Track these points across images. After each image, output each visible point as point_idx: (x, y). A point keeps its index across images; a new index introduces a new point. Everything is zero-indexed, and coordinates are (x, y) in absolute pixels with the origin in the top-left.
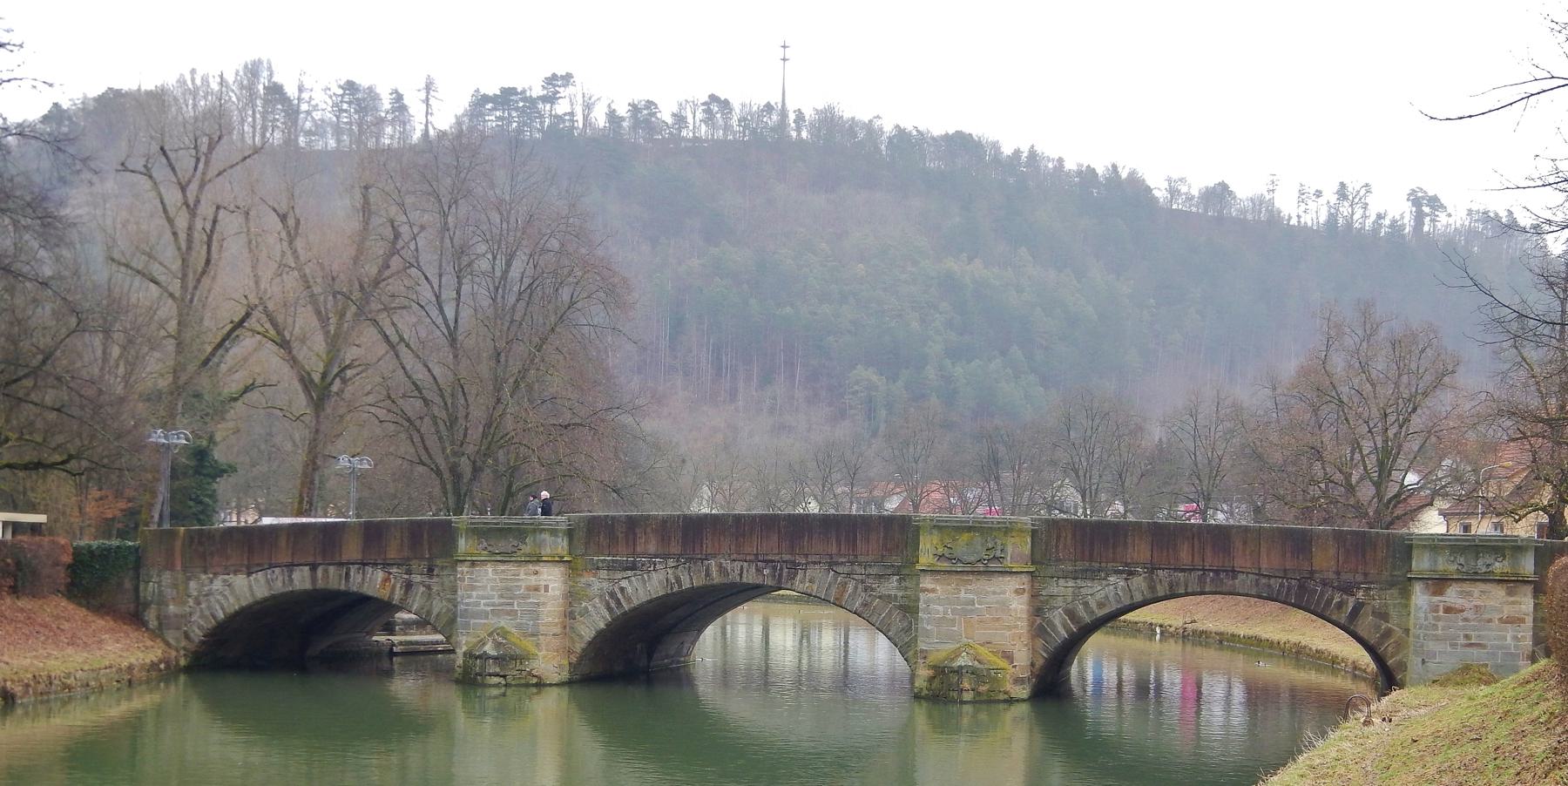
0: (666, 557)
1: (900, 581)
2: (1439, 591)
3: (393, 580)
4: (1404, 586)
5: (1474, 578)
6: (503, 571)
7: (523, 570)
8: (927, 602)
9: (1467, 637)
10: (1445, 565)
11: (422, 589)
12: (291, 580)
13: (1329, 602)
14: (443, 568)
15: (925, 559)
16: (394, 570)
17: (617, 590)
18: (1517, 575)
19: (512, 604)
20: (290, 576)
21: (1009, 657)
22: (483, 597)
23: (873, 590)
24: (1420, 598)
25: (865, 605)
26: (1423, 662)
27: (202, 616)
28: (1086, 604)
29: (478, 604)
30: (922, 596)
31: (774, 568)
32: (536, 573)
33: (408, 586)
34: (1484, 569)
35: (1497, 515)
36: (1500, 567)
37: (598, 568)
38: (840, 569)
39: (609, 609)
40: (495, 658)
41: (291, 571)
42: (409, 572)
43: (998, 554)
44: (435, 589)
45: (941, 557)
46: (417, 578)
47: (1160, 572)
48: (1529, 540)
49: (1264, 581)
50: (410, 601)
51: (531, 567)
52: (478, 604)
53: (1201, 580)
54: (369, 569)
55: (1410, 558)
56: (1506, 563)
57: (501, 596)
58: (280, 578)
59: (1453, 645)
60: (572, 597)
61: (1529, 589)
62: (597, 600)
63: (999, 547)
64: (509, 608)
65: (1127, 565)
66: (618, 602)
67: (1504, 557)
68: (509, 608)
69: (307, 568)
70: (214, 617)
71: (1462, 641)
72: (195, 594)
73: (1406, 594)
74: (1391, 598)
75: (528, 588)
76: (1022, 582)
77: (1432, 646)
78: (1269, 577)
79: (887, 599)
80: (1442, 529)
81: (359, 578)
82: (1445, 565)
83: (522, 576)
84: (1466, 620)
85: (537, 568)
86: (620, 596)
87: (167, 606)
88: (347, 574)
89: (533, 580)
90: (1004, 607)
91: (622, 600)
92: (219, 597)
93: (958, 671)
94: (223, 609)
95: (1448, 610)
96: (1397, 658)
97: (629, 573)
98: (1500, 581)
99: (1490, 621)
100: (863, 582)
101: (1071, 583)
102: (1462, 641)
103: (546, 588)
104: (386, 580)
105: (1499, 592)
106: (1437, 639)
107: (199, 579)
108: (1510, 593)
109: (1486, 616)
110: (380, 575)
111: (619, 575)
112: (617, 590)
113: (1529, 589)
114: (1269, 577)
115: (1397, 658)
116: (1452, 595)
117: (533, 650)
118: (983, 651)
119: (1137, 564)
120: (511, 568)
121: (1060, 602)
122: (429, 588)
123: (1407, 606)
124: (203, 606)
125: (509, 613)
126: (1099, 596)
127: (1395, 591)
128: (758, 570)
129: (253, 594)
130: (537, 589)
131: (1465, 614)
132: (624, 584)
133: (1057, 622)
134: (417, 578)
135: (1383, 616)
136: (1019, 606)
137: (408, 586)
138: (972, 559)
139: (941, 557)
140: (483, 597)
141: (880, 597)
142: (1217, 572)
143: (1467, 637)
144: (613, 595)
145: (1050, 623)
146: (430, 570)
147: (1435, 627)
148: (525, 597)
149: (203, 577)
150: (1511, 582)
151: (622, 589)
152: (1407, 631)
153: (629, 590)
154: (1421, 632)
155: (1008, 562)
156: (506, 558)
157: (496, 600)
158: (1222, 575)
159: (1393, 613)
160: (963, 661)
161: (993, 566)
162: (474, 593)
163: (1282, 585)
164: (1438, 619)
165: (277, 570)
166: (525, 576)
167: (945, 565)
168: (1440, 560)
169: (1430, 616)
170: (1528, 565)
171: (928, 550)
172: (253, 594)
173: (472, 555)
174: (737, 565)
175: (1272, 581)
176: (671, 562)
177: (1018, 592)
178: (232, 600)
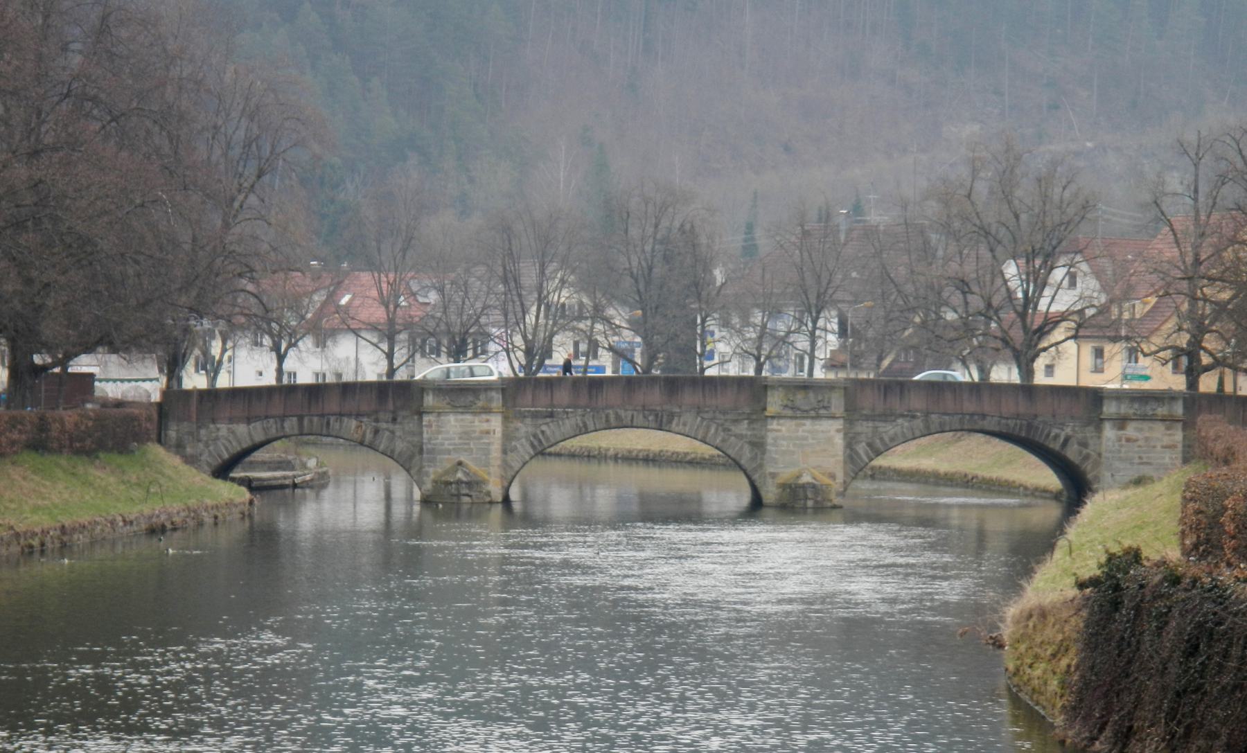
0: (576, 407)
1: (749, 424)
2: (1122, 428)
3: (364, 427)
4: (1098, 422)
5: (1144, 418)
6: (462, 420)
7: (477, 419)
8: (775, 439)
9: (1140, 458)
10: (1125, 409)
11: (387, 433)
12: (283, 428)
13: (1048, 435)
14: (404, 418)
15: (772, 409)
16: (365, 419)
17: (538, 432)
18: (1172, 416)
19: (469, 444)
20: (282, 425)
21: (833, 476)
22: (447, 439)
23: (729, 430)
24: (1109, 432)
25: (723, 441)
26: (1112, 475)
27: (210, 454)
28: (882, 439)
29: (442, 444)
30: (769, 434)
31: (657, 416)
32: (488, 421)
33: (376, 432)
34: (1151, 413)
35: (96, 246)
36: (1162, 411)
37: (525, 417)
38: (706, 416)
39: (533, 446)
40: (467, 483)
41: (283, 421)
42: (377, 420)
43: (826, 404)
44: (398, 434)
45: (786, 406)
46: (383, 425)
47: (933, 416)
48: (1180, 392)
49: (1004, 421)
50: (377, 442)
51: (484, 417)
52: (442, 444)
53: (961, 421)
54: (345, 419)
55: (1101, 405)
56: (1165, 408)
57: (460, 438)
58: (274, 426)
59: (1132, 464)
60: (508, 437)
61: (1180, 425)
62: (524, 440)
63: (826, 400)
64: (466, 447)
65: (909, 411)
66: (540, 441)
67: (1164, 404)
68: (466, 447)
69: (295, 419)
70: (220, 456)
71: (1137, 461)
72: (205, 439)
73: (1099, 429)
74: (1090, 432)
75: (482, 432)
76: (839, 424)
77: (1117, 464)
78: (1007, 418)
79: (740, 437)
80: (822, 376)
81: (337, 426)
82: (1125, 409)
83: (477, 423)
84: (1139, 446)
85: (488, 417)
86: (541, 436)
87: (185, 448)
88: (328, 423)
89: (485, 426)
90: (830, 440)
91: (543, 440)
92: (224, 441)
93: (803, 486)
94: (227, 449)
95: (1128, 440)
96: (1095, 473)
97: (548, 420)
98: (1161, 420)
99: (1154, 447)
100: (722, 425)
101: (870, 424)
102: (1137, 461)
103: (494, 431)
104: (358, 427)
105: (1160, 427)
106: (1120, 459)
107: (208, 427)
108: (1168, 428)
109: (1152, 444)
110: (354, 423)
111: (540, 421)
112: (538, 432)
113: (1180, 425)
114: (1007, 418)
115: (1095, 473)
116: (1131, 430)
117: (486, 477)
118: (816, 473)
119: (917, 411)
120: (468, 417)
121: (863, 437)
122: (393, 432)
123: (1099, 437)
124: (211, 448)
125: (466, 450)
126: (892, 432)
127: (1091, 428)
128: (645, 417)
129: (252, 440)
130: (488, 432)
131: (1140, 443)
132: (544, 428)
133: (861, 452)
134: (383, 425)
135: (1084, 444)
136: (839, 441)
137: (376, 432)
138: (807, 408)
139: (786, 406)
140: (447, 439)
141: (735, 436)
142: (972, 415)
143: (1140, 458)
144: (535, 436)
145: (857, 454)
146: (394, 420)
147: (1119, 451)
148: (480, 438)
149: (212, 426)
150: (1169, 420)
151: (543, 432)
152: (1100, 455)
153: (548, 432)
154: (1110, 455)
155: (833, 410)
156: (467, 409)
157: (457, 441)
158: (976, 417)
159: (1091, 442)
160: (806, 479)
161: (822, 412)
162: (440, 437)
163: (1016, 424)
164: (1121, 446)
165: (272, 421)
166: (478, 423)
167: (789, 412)
168: (1123, 407)
169: (1116, 444)
170: (1179, 409)
171: (774, 403)
172: (252, 440)
173: (439, 408)
174: (630, 413)
175: (1009, 421)
176: (580, 411)
177: (838, 431)
178: (234, 443)
